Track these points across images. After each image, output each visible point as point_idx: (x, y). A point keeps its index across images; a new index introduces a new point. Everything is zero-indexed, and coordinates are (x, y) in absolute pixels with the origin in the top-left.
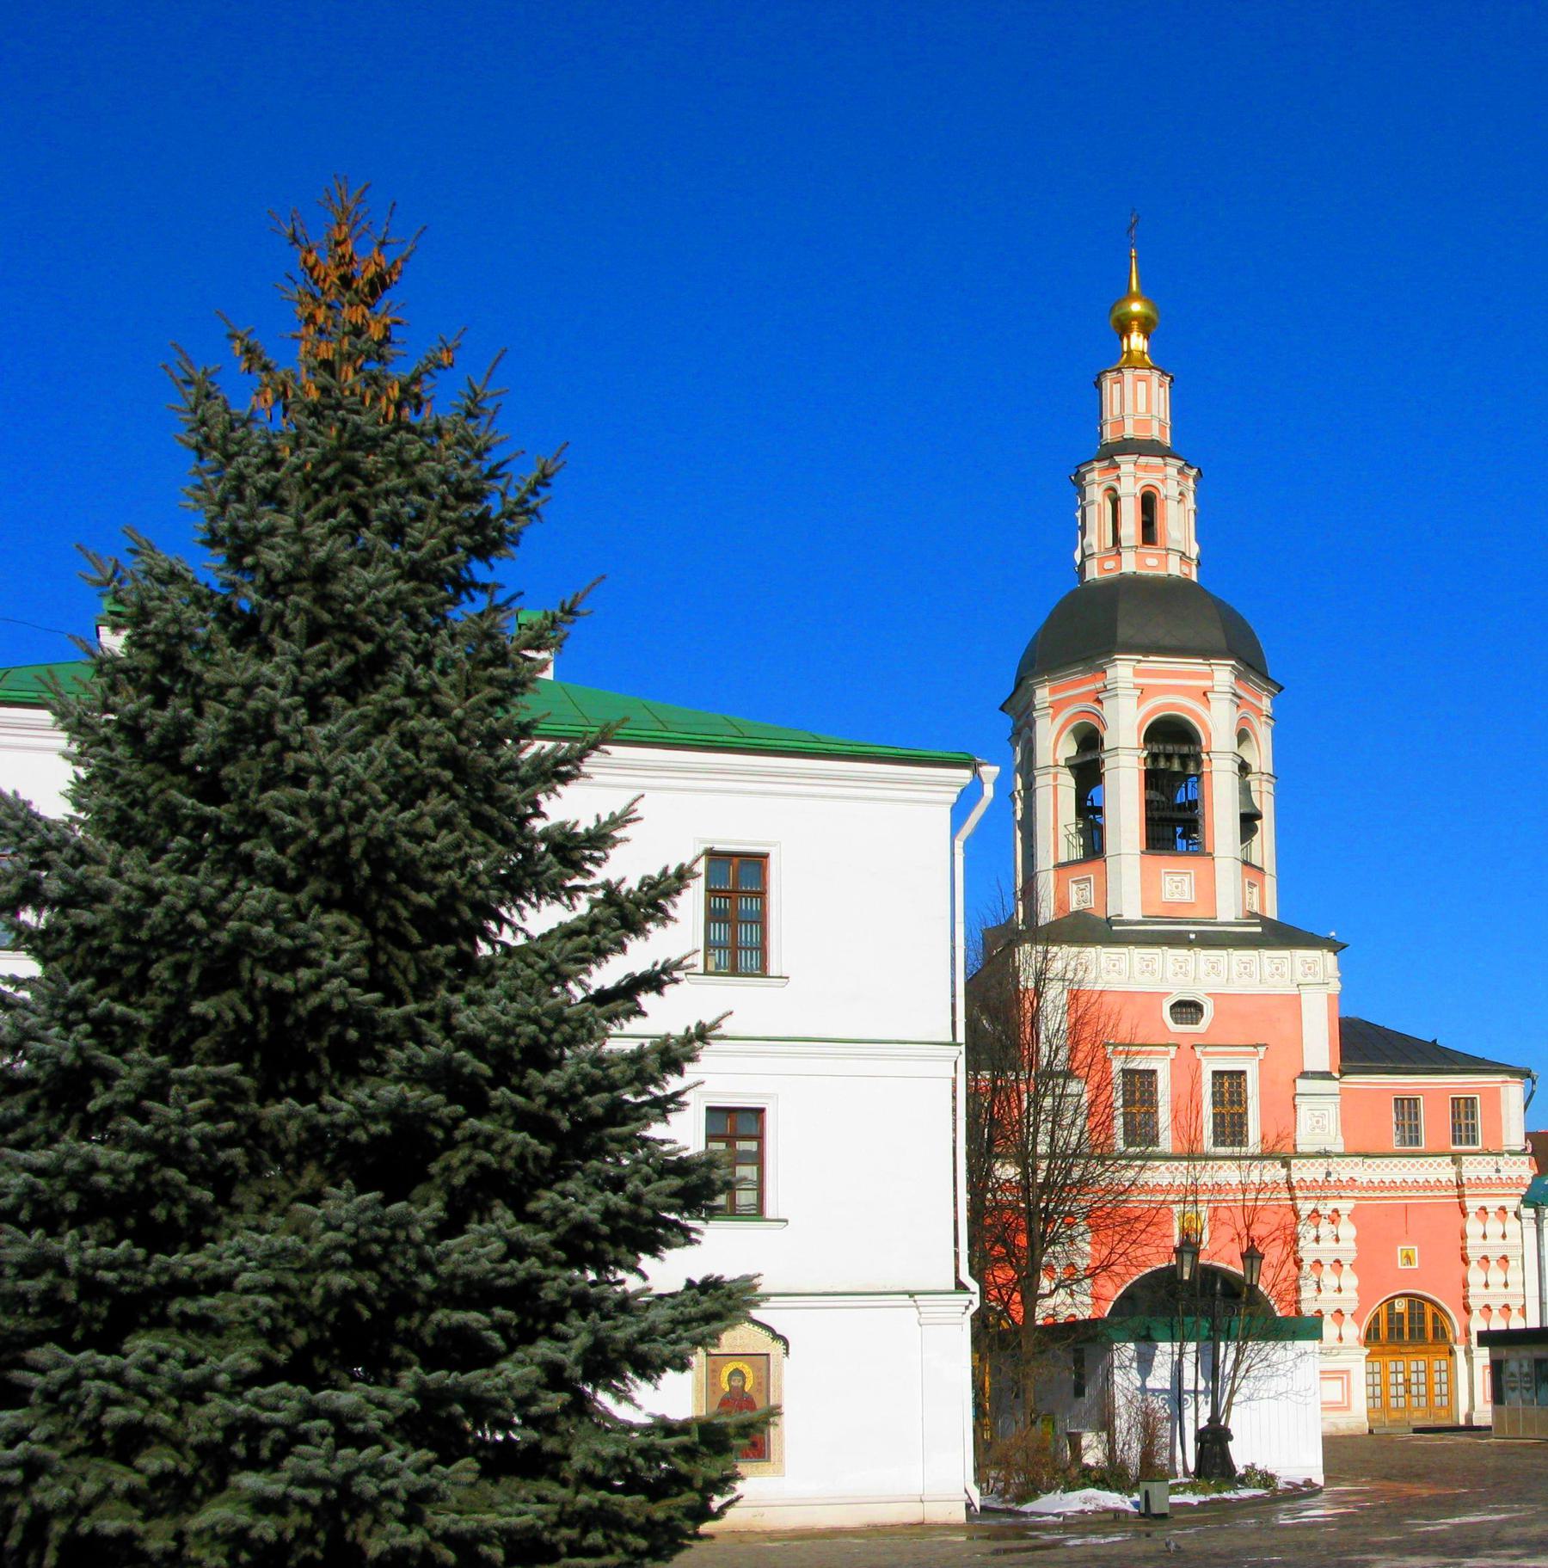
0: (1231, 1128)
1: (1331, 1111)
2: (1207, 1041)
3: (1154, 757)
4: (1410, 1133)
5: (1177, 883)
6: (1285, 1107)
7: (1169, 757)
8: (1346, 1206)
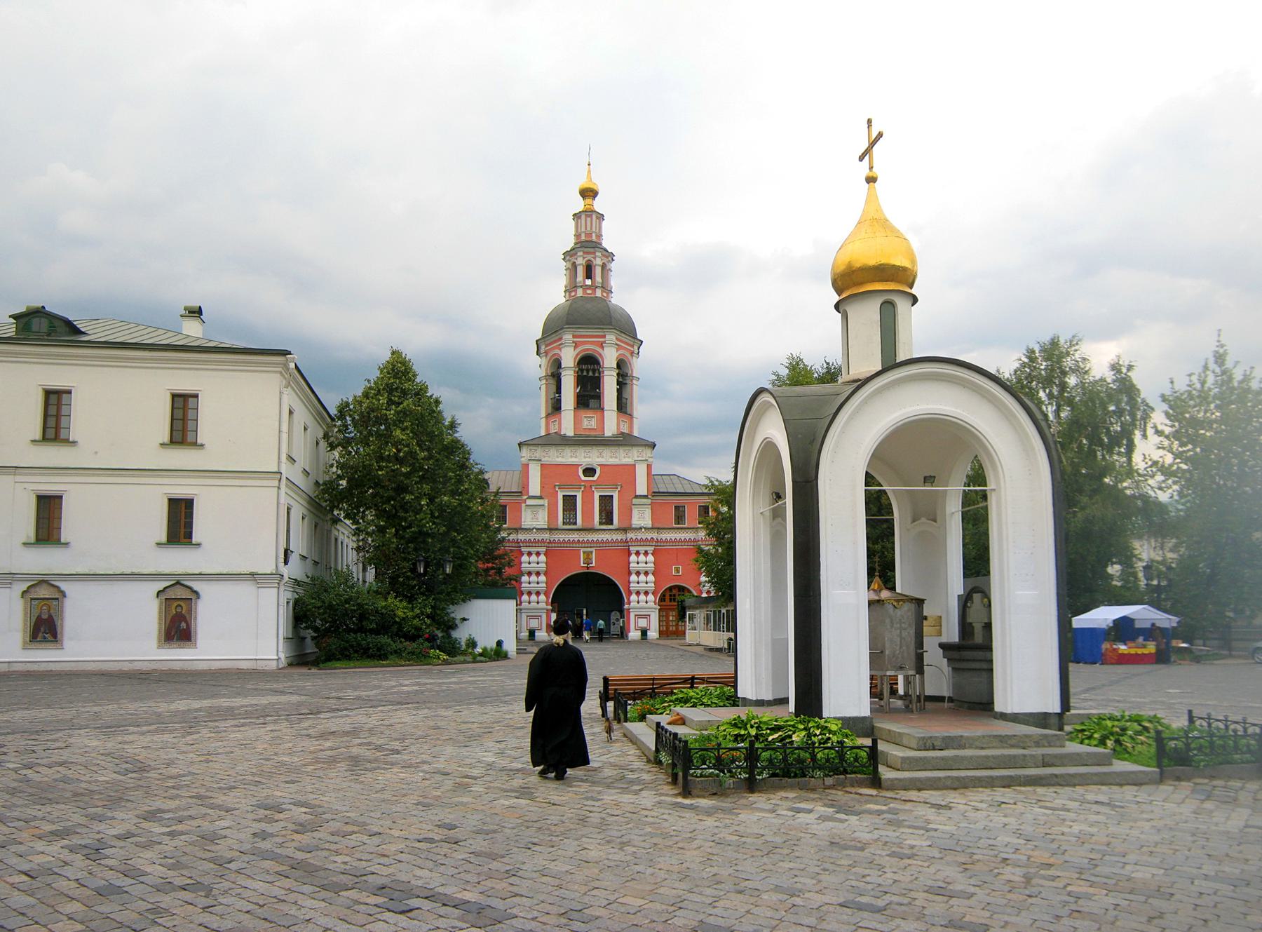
0: (607, 517)
1: (648, 513)
2: (598, 484)
3: (582, 370)
4: (679, 518)
5: (589, 422)
6: (627, 512)
7: (588, 371)
8: (650, 549)
